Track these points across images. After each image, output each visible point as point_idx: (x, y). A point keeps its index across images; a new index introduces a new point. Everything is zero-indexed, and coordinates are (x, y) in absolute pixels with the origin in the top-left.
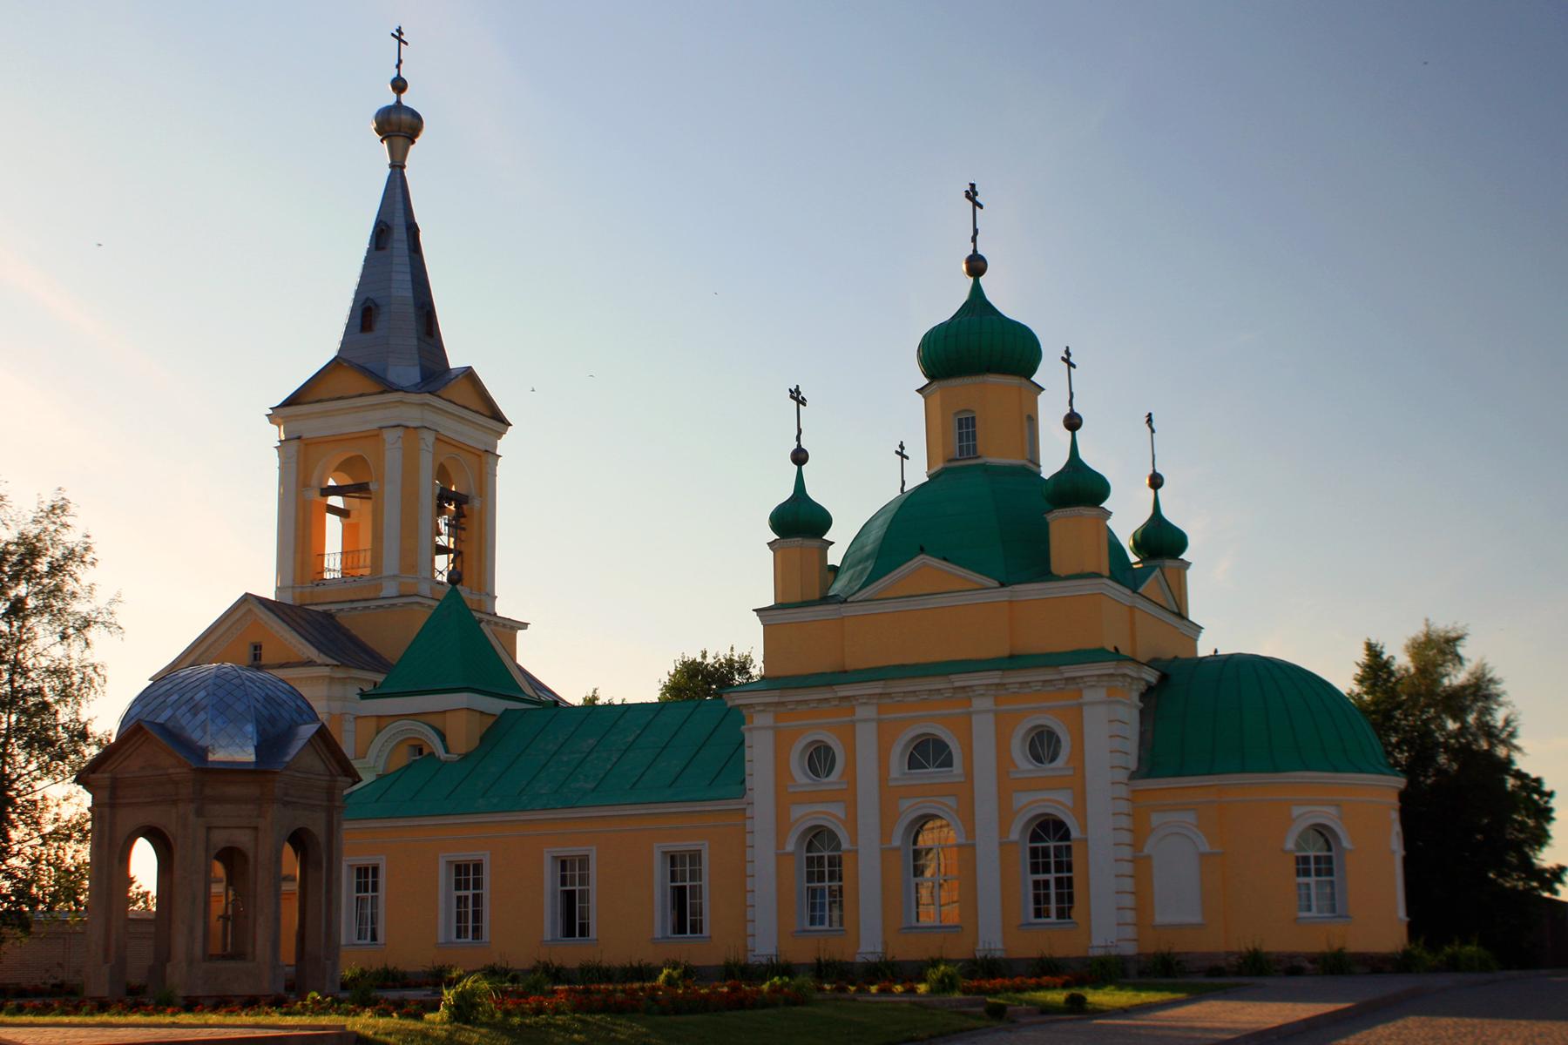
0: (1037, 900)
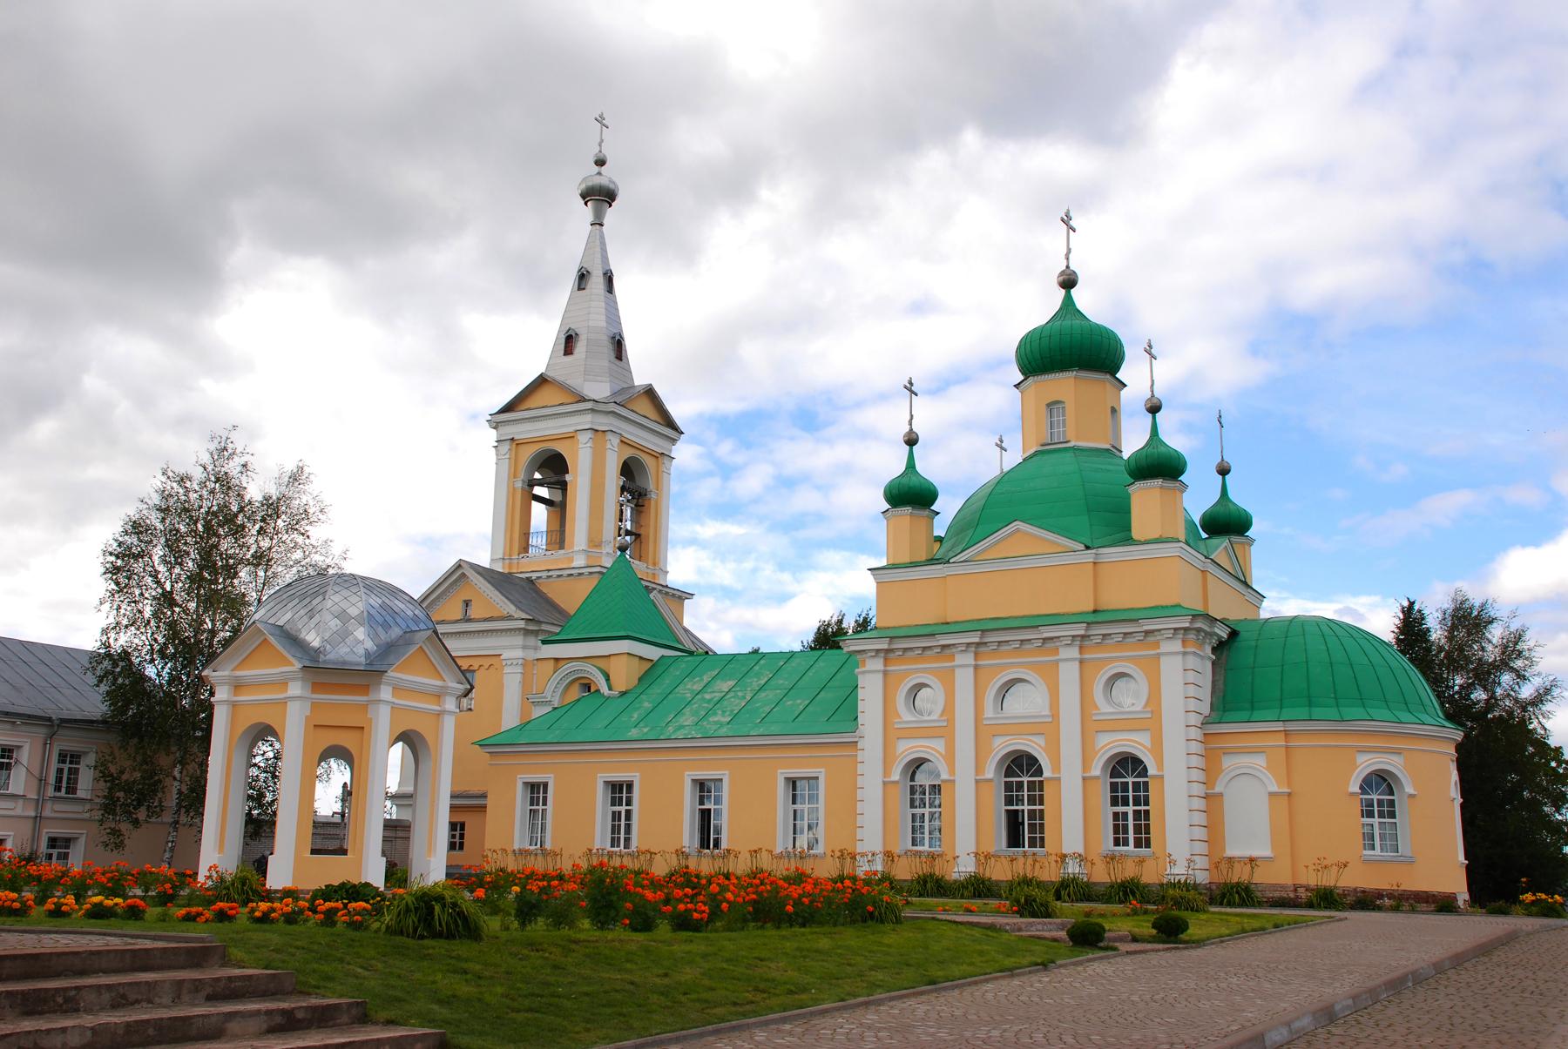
0: (1116, 829)
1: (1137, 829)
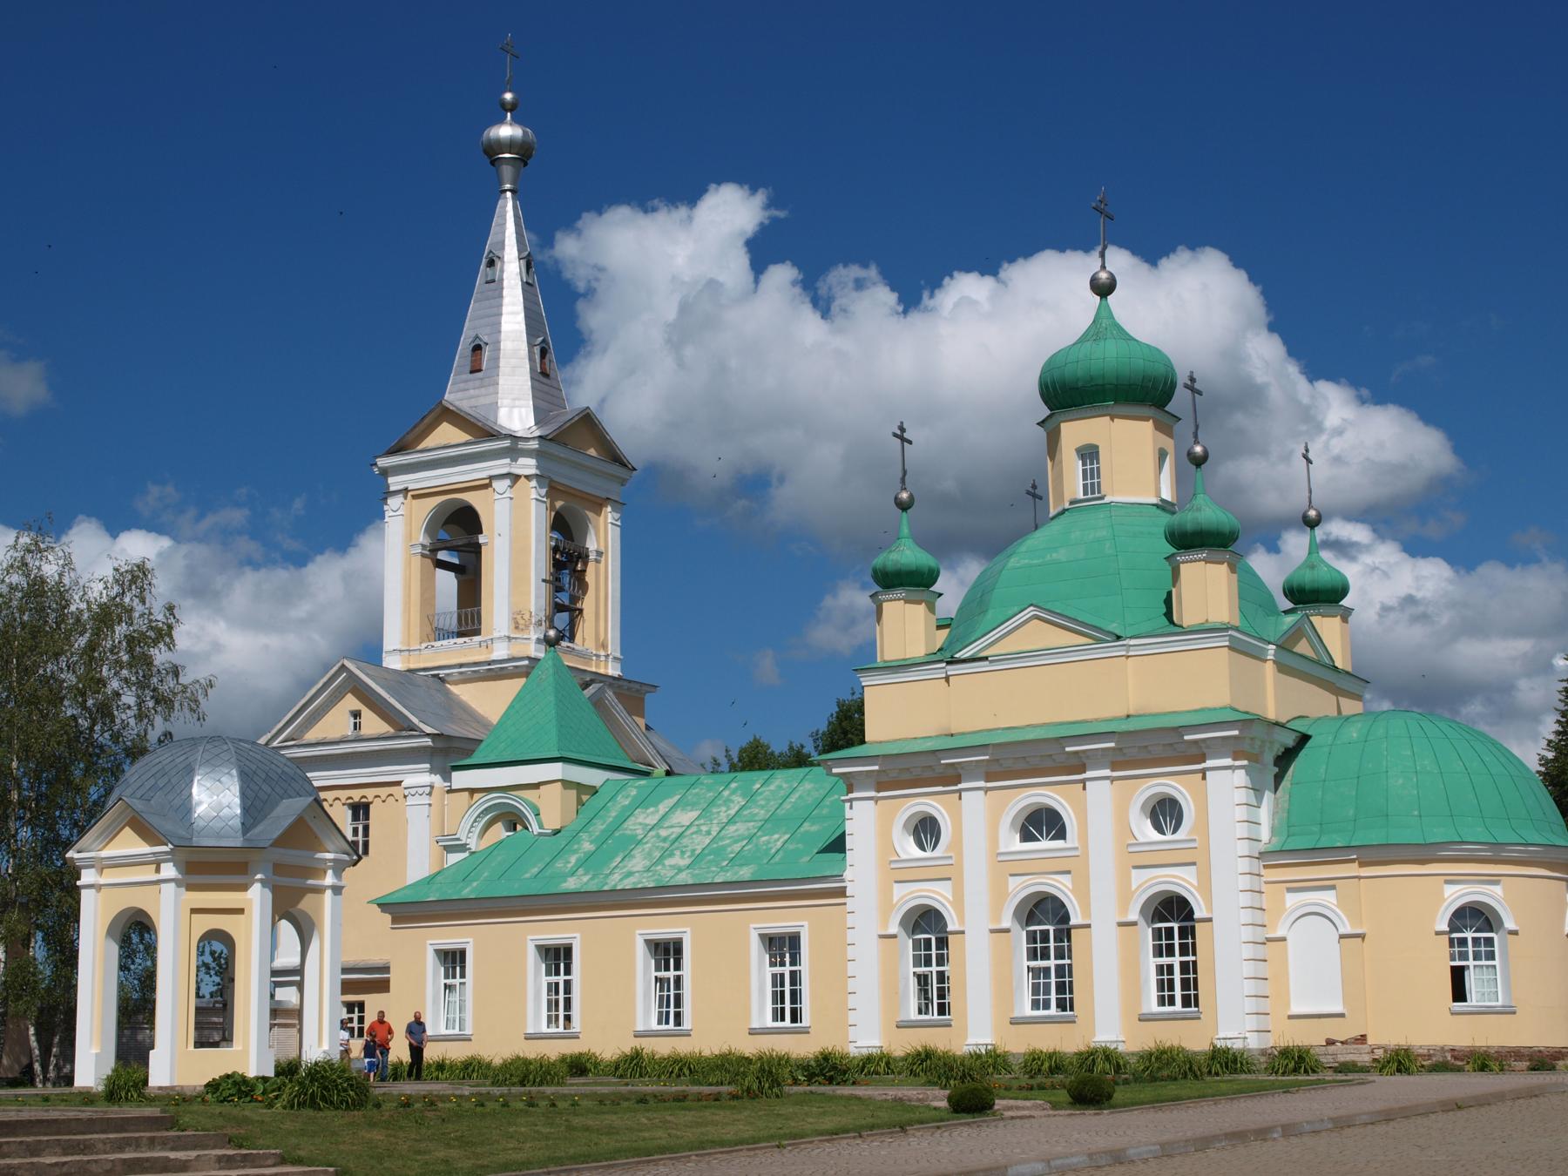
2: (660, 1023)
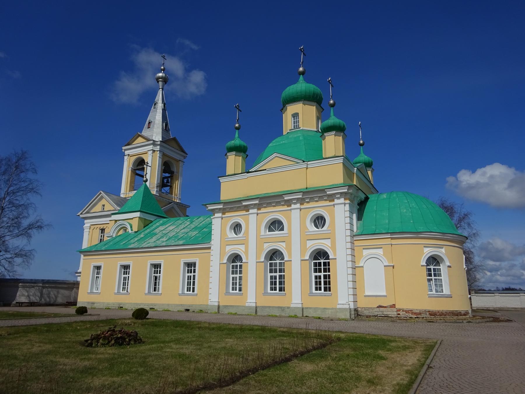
1: (325, 283)
2: (187, 291)
